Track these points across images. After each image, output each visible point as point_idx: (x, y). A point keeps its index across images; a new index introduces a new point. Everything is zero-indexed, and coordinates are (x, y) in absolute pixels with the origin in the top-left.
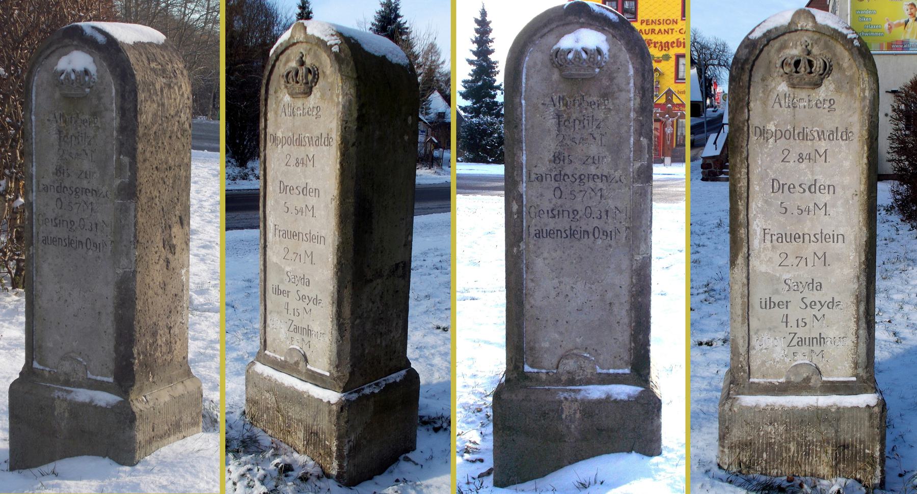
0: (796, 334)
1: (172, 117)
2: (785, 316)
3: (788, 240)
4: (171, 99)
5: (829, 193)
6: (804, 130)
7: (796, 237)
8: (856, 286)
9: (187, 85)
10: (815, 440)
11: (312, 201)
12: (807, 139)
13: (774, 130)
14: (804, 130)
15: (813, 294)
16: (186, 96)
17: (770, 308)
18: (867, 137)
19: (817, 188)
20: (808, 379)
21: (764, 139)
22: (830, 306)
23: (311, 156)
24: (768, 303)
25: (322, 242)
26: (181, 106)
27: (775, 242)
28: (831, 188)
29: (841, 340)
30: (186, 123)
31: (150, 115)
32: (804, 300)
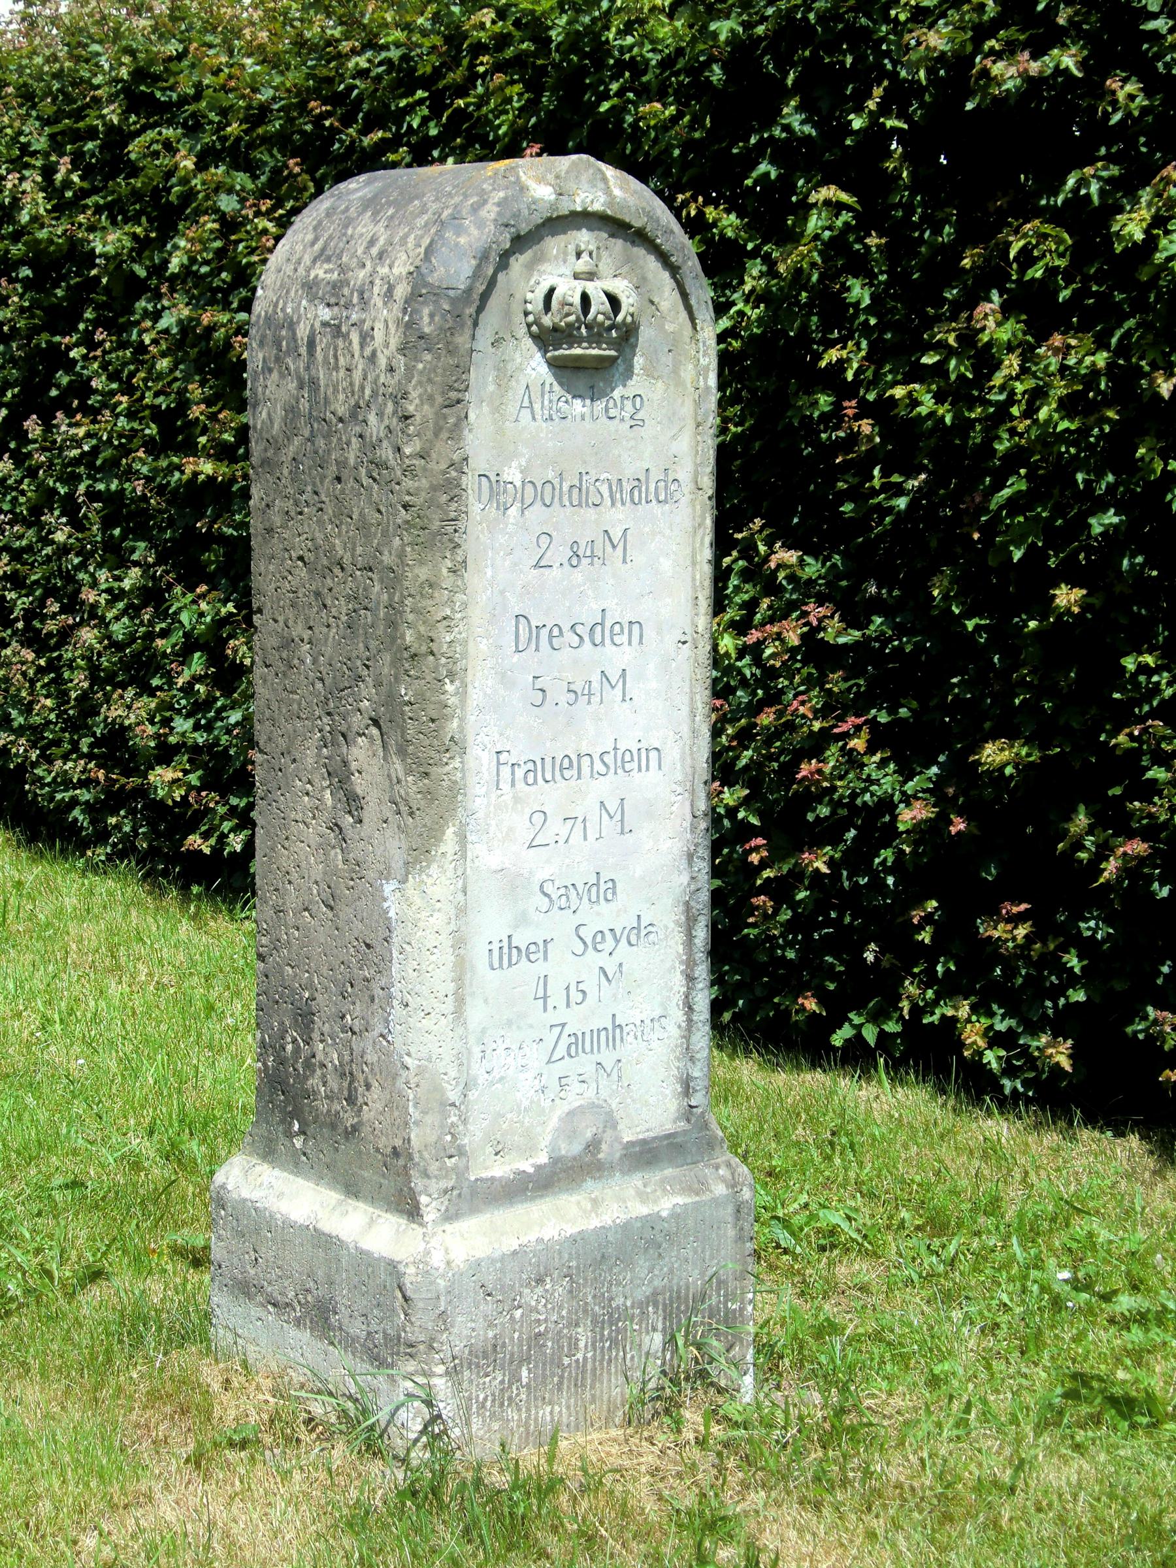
0: (563, 1025)
1: (341, 420)
4: (336, 368)
5: (630, 643)
6: (581, 480)
7: (568, 766)
8: (685, 879)
10: (629, 1304)
11: (617, 657)
12: (587, 505)
13: (518, 484)
14: (581, 480)
15: (598, 914)
16: (382, 361)
17: (510, 965)
18: (710, 492)
20: (593, 1146)
21: (498, 508)
22: (633, 940)
23: (616, 535)
24: (506, 950)
25: (654, 764)
26: (368, 392)
27: (520, 785)
29: (656, 1024)
30: (385, 444)
31: (280, 412)
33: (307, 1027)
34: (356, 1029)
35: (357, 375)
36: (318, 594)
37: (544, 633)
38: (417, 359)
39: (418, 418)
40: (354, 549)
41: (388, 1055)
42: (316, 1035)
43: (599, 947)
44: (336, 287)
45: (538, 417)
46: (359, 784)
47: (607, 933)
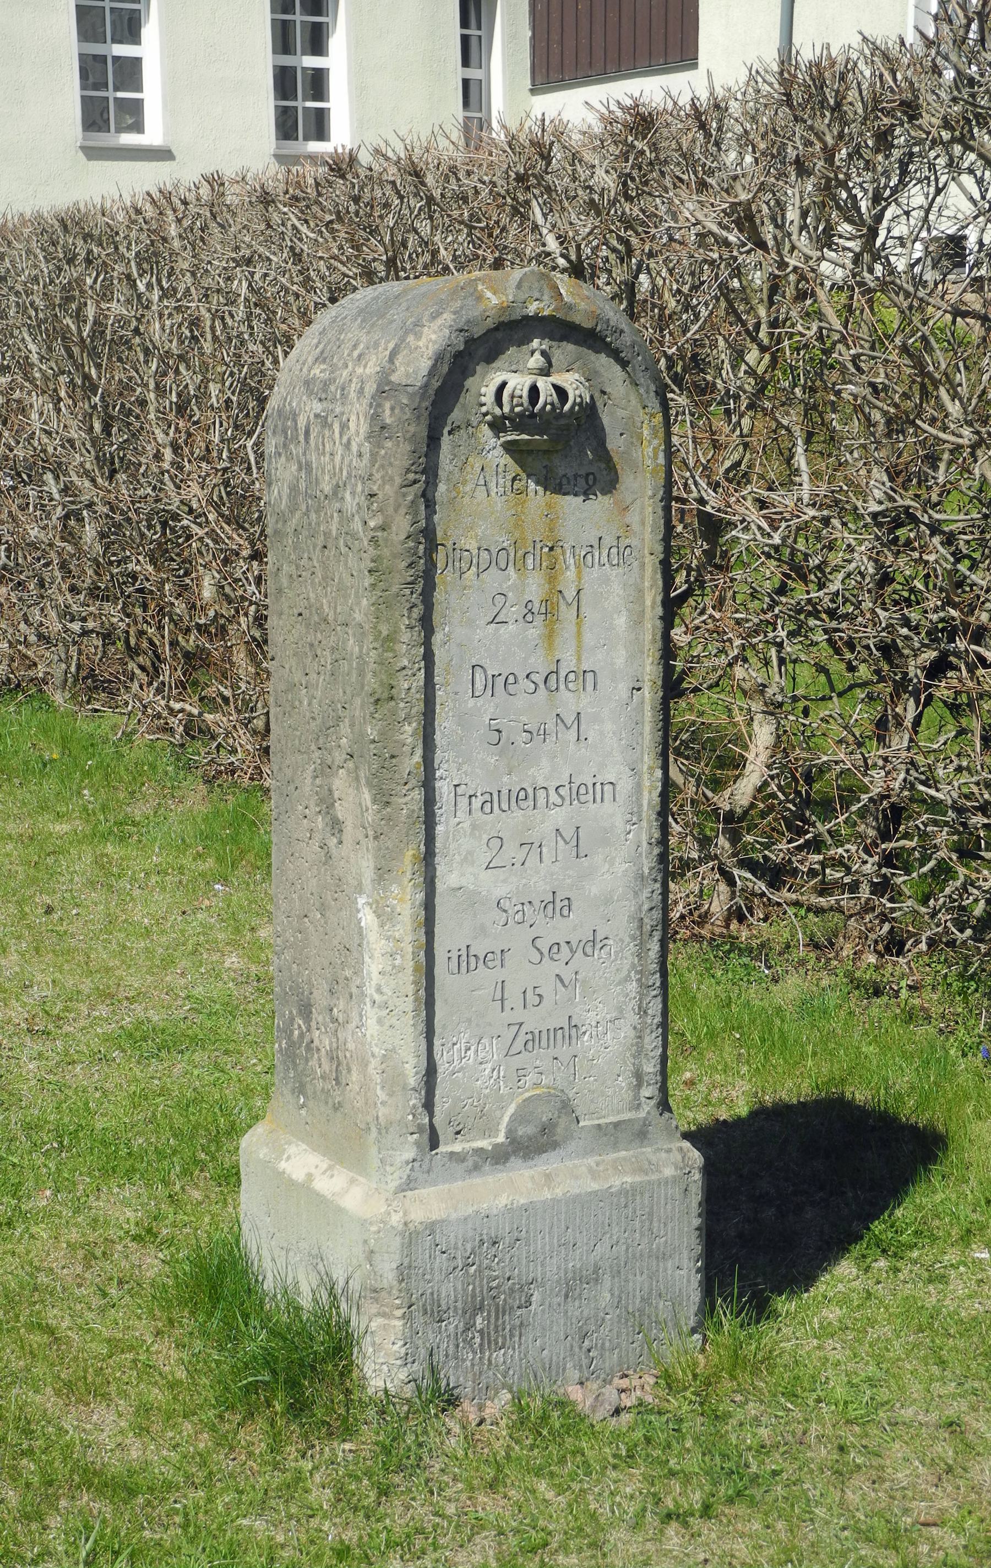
0: (521, 1024)
2: (500, 985)
3: (505, 806)
7: (520, 797)
9: (362, 419)
19: (562, 679)
22: (589, 950)
26: (345, 473)
28: (590, 676)
30: (357, 518)
31: (286, 490)
32: (538, 942)
33: (308, 1016)
34: (340, 1020)
35: (338, 458)
36: (312, 645)
37: (500, 681)
38: (380, 446)
39: (380, 496)
40: (335, 608)
41: (363, 1044)
42: (313, 1024)
43: (556, 957)
44: (326, 385)
45: (493, 494)
46: (340, 810)
47: (563, 945)
